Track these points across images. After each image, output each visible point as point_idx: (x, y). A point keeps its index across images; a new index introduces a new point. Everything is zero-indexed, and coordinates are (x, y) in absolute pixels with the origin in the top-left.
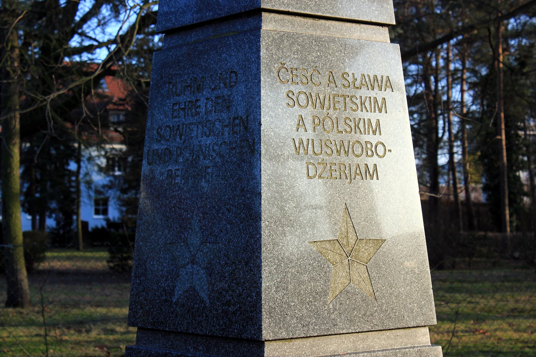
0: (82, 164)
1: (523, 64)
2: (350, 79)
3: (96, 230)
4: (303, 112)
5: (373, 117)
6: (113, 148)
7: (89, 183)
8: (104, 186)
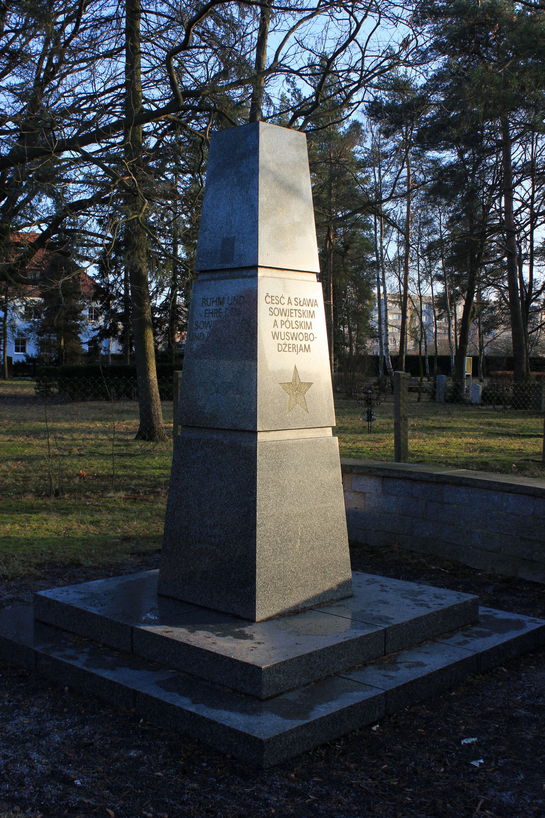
0: (8, 312)
1: (347, 247)
2: (298, 301)
3: (18, 364)
4: (276, 318)
5: (309, 320)
6: (34, 300)
7: (13, 327)
8: (26, 330)
